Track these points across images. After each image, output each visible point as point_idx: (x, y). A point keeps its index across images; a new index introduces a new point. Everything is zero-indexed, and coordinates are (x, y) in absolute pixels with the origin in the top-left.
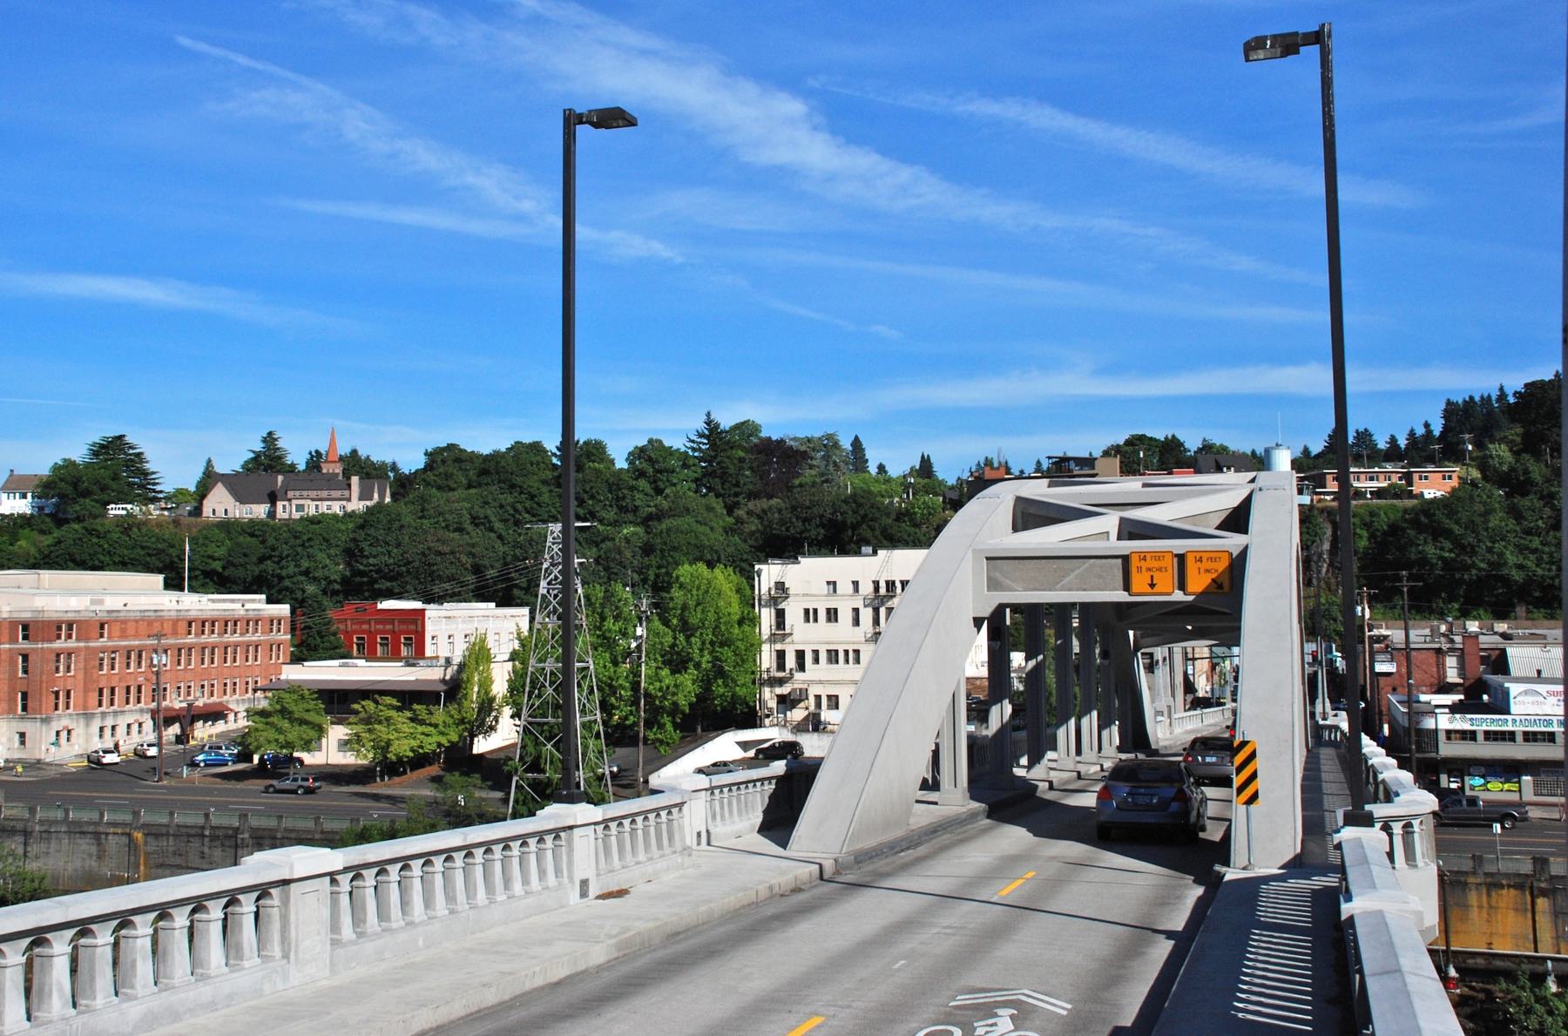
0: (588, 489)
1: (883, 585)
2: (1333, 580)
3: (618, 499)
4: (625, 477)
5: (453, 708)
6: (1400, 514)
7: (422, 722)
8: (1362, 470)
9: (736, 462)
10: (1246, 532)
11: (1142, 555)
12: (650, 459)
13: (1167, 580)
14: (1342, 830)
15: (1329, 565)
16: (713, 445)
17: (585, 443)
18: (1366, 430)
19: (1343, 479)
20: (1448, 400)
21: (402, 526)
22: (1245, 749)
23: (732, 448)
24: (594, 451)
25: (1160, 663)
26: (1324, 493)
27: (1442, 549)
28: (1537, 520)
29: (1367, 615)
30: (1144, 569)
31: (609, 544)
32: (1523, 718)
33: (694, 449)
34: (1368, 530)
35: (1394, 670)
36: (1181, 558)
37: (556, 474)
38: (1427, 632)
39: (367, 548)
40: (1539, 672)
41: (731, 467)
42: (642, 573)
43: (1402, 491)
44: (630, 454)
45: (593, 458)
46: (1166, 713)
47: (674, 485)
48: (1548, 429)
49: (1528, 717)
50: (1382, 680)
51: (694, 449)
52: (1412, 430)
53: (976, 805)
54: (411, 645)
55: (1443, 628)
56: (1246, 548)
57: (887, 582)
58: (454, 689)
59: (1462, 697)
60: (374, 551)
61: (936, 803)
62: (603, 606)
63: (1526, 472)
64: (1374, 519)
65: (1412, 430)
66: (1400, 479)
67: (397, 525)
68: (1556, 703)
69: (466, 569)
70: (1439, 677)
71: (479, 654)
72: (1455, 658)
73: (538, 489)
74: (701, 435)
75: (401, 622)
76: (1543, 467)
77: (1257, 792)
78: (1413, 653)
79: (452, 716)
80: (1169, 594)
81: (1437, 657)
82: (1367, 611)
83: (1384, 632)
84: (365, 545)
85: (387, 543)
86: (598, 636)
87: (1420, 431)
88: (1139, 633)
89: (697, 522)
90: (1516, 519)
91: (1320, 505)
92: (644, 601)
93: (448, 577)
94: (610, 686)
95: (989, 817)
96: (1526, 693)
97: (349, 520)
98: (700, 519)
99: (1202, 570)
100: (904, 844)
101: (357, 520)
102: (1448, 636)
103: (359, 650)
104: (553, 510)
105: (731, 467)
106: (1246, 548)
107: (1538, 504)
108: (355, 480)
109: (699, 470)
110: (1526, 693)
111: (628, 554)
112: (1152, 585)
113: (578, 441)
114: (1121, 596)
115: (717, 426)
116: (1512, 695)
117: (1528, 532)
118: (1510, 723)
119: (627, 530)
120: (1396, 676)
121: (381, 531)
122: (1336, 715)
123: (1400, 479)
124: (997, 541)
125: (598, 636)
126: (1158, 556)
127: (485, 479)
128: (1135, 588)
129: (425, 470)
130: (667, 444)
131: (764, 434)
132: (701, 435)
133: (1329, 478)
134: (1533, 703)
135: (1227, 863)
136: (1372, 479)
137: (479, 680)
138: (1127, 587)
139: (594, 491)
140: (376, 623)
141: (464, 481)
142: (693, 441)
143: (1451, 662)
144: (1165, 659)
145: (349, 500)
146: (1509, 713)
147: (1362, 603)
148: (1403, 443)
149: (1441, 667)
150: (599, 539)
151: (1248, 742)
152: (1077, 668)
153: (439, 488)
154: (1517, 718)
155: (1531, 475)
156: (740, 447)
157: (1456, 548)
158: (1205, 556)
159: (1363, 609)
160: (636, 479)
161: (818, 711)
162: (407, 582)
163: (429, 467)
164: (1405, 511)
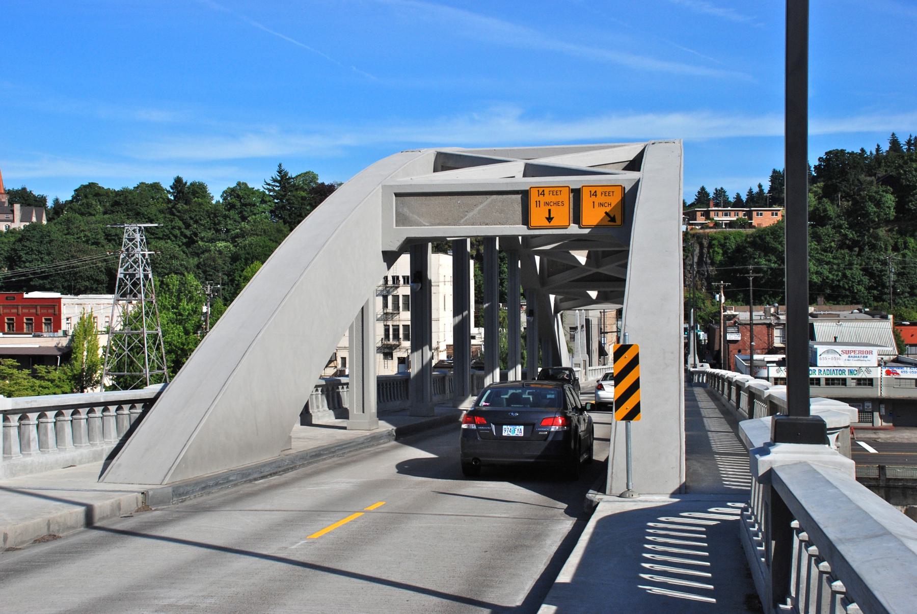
0: (193, 217)
1: (390, 279)
2: (699, 283)
3: (215, 224)
4: (221, 208)
5: (67, 368)
6: (744, 238)
7: (41, 378)
8: (720, 209)
9: (299, 199)
10: (639, 170)
11: (541, 190)
12: (238, 196)
13: (562, 214)
14: (773, 450)
15: (697, 272)
16: (283, 187)
17: (191, 184)
18: (722, 188)
19: (706, 214)
20: (774, 170)
21: (52, 241)
22: (626, 355)
23: (297, 190)
24: (199, 191)
25: (579, 329)
26: (695, 224)
27: (769, 261)
28: (831, 242)
29: (723, 301)
30: (542, 204)
31: (207, 255)
32: (826, 369)
33: (270, 190)
34: (722, 249)
35: (739, 339)
36: (577, 193)
37: (170, 206)
38: (762, 313)
39: (24, 256)
40: (835, 338)
41: (296, 203)
42: (231, 275)
43: (745, 223)
44: (224, 192)
45: (197, 195)
46: (582, 366)
47: (255, 214)
48: (840, 183)
49: (829, 368)
50: (731, 346)
51: (270, 190)
52: (751, 189)
53: (385, 427)
54: (50, 324)
55: (772, 310)
56: (639, 181)
57: (393, 277)
58: (67, 354)
59: (784, 356)
60: (29, 258)
61: (345, 428)
62: (179, 291)
63: (825, 210)
64: (727, 241)
65: (751, 189)
66: (745, 215)
67: (47, 239)
68: (847, 358)
69: (101, 271)
70: (769, 343)
71: (86, 327)
72: (779, 331)
73: (155, 215)
75: (42, 307)
76: (835, 207)
77: (638, 380)
78: (754, 327)
79: (65, 373)
80: (565, 227)
81: (768, 330)
82: (723, 298)
83: (733, 313)
84: (22, 253)
85: (39, 252)
86: (175, 313)
87: (756, 190)
88: (560, 297)
89: (270, 240)
90: (817, 241)
91: (692, 232)
92: (209, 286)
93: (88, 277)
94: (182, 350)
95: (396, 440)
96: (828, 352)
97: (10, 235)
98: (272, 238)
99: (596, 204)
100: (267, 470)
101: (17, 235)
102: (776, 315)
103: (9, 327)
104: (166, 230)
105: (296, 203)
106: (639, 181)
107: (831, 231)
108: (17, 207)
109: (273, 205)
110: (828, 352)
111: (220, 261)
112: (549, 219)
113: (186, 183)
114: (520, 230)
115: (286, 174)
116: (818, 354)
117: (825, 250)
118: (817, 372)
119: (221, 245)
120: (740, 343)
121: (35, 243)
122: (702, 366)
123: (745, 215)
124: (408, 179)
125: (175, 313)
126: (555, 190)
127: (117, 208)
128: (534, 221)
129: (71, 202)
130: (250, 186)
131: (320, 181)
132: (275, 181)
133: (699, 214)
134: (832, 359)
135: (602, 489)
136: (726, 215)
137: (88, 347)
138: (526, 221)
139: (198, 218)
140: (23, 308)
141: (102, 209)
142: (269, 184)
143: (777, 333)
144: (582, 326)
145: (13, 221)
146: (816, 366)
147: (720, 292)
148: (744, 198)
149: (770, 336)
150: (199, 252)
151: (630, 346)
152: (524, 337)
153: (82, 214)
154: (822, 369)
155: (829, 212)
156: (302, 189)
157: (778, 260)
158: (599, 190)
159: (720, 297)
160: (229, 210)
161: (343, 369)
162: (55, 281)
163: (75, 198)
164: (747, 236)
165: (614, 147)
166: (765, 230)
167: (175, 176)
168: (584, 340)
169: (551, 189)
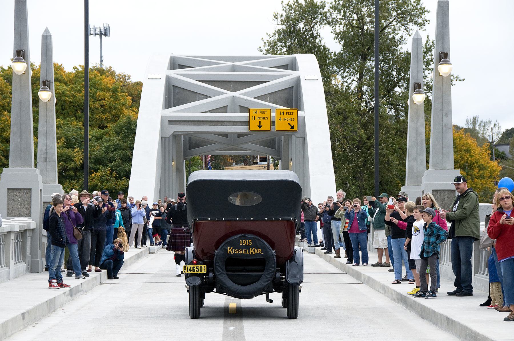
167: (142, 82)
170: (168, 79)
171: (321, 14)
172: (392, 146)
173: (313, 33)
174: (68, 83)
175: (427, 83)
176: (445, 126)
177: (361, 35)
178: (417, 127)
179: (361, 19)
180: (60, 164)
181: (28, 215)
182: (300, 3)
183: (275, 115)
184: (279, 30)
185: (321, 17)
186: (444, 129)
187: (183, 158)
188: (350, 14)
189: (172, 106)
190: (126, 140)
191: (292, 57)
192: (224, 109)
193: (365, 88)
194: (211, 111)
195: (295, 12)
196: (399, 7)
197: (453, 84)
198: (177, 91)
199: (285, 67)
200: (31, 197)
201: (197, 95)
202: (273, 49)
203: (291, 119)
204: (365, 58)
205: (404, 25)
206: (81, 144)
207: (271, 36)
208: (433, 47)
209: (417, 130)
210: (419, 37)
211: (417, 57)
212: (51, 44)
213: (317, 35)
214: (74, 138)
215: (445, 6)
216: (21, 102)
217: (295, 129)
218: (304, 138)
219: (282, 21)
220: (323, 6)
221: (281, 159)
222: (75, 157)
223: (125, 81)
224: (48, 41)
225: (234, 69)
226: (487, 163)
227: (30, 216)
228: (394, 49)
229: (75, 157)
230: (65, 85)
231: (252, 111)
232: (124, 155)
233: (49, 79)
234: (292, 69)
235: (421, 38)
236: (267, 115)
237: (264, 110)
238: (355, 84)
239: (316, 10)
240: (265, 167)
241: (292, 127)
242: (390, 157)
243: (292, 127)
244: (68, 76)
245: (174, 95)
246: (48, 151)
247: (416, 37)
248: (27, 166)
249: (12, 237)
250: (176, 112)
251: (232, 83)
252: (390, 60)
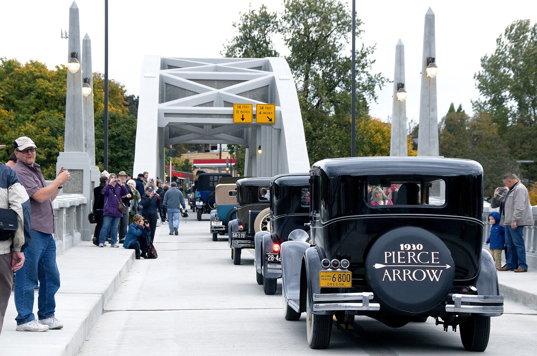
30: (239, 112)
74: (480, 91)
132: (480, 91)
165: (185, 59)
166: (128, 97)
168: (372, 173)
169: (243, 105)
170: (162, 78)
171: (273, 23)
172: (333, 138)
173: (266, 39)
174: (51, 79)
175: (362, 84)
176: (432, 119)
177: (307, 42)
178: (400, 120)
179: (307, 27)
180: (46, 150)
181: (81, 192)
182: (254, 13)
183: (256, 110)
184: (237, 37)
185: (273, 26)
186: (431, 121)
187: (164, 146)
188: (298, 24)
189: (165, 101)
190: (102, 130)
191: (263, 60)
192: (210, 104)
193: (310, 87)
194: (200, 105)
195: (251, 21)
196: (339, 18)
197: (384, 85)
198: (169, 88)
199: (259, 68)
200: (83, 177)
201: (187, 91)
202: (230, 53)
203: (269, 113)
204: (310, 61)
205: (343, 34)
206: (61, 133)
207: (230, 42)
208: (367, 53)
209: (400, 124)
210: (401, 44)
211: (400, 62)
212: (90, 47)
213: (270, 41)
214: (56, 127)
215: (431, 18)
216: (74, 96)
217: (273, 121)
218: (281, 129)
219: (240, 29)
220: (275, 16)
221: (248, 147)
222: (58, 145)
223: (100, 79)
224: (88, 45)
225: (216, 69)
226: (410, 152)
227: (82, 193)
228: (335, 55)
229: (58, 145)
230: (48, 81)
231: (236, 106)
232: (100, 143)
233: (88, 77)
234: (265, 70)
235: (403, 46)
236: (249, 109)
237: (246, 105)
238: (302, 83)
239: (269, 20)
240: (217, 155)
241: (271, 120)
242: (332, 146)
243: (271, 120)
244: (50, 73)
245: (167, 91)
246: (87, 138)
247: (399, 44)
248: (80, 151)
249: (64, 212)
250: (170, 106)
251: (216, 82)
252: (331, 64)
